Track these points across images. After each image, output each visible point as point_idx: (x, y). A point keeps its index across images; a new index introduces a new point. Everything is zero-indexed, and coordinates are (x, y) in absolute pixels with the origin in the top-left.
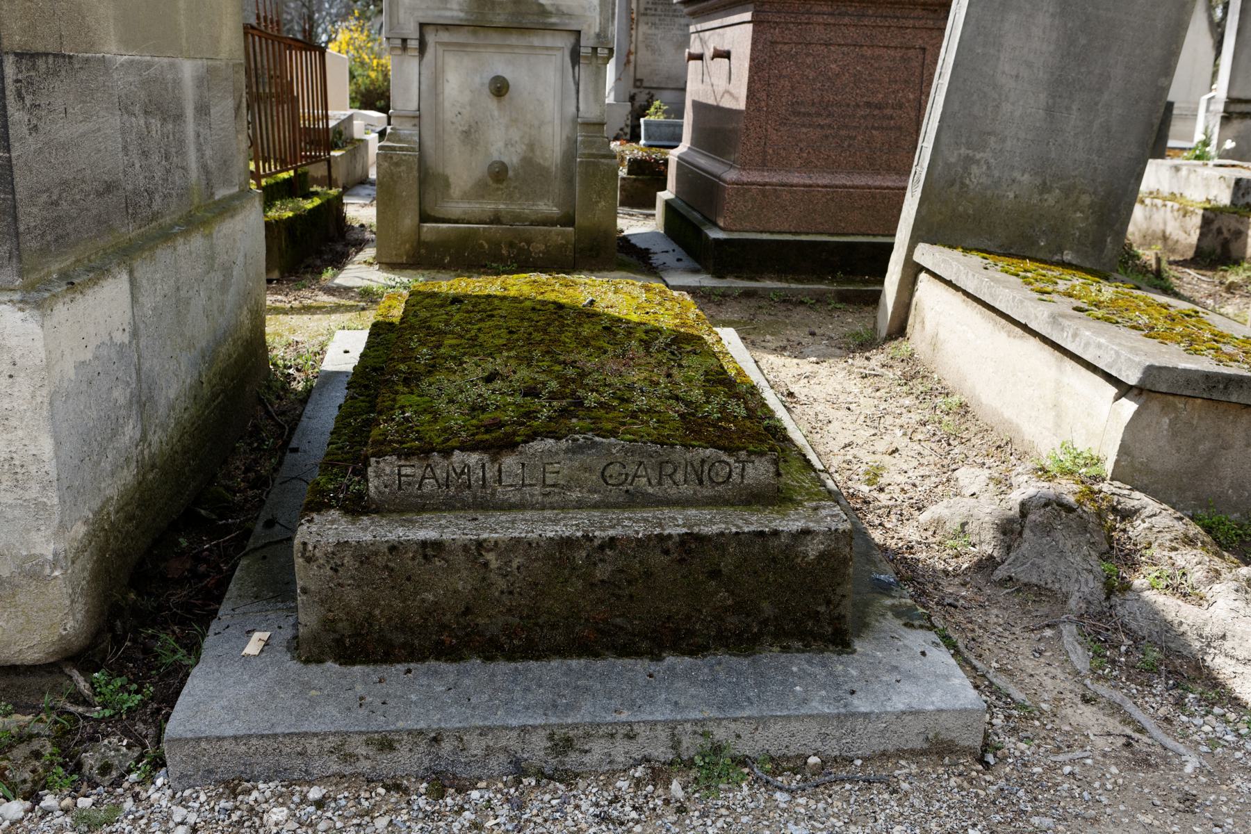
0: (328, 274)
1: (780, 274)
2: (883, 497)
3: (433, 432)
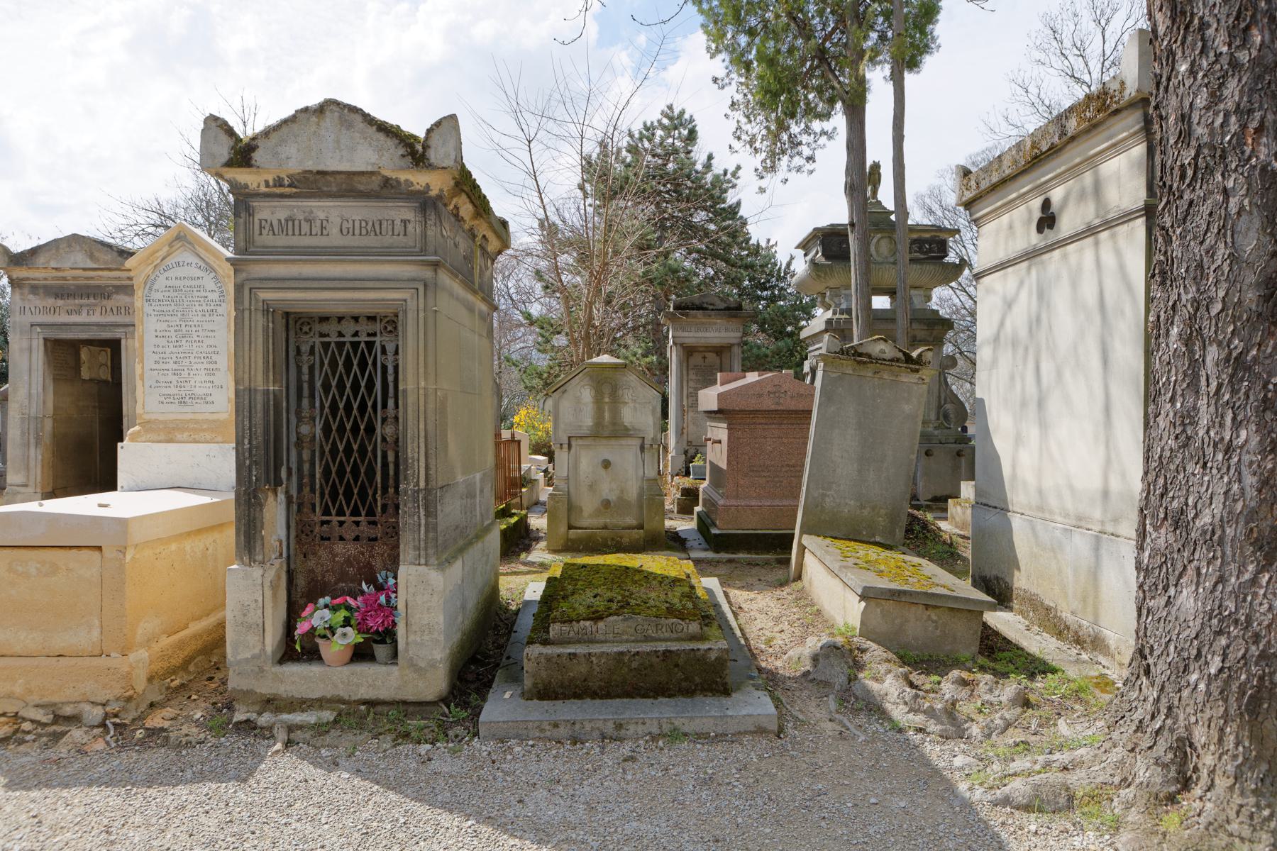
0: (523, 555)
1: (749, 551)
2: (771, 650)
3: (573, 615)
